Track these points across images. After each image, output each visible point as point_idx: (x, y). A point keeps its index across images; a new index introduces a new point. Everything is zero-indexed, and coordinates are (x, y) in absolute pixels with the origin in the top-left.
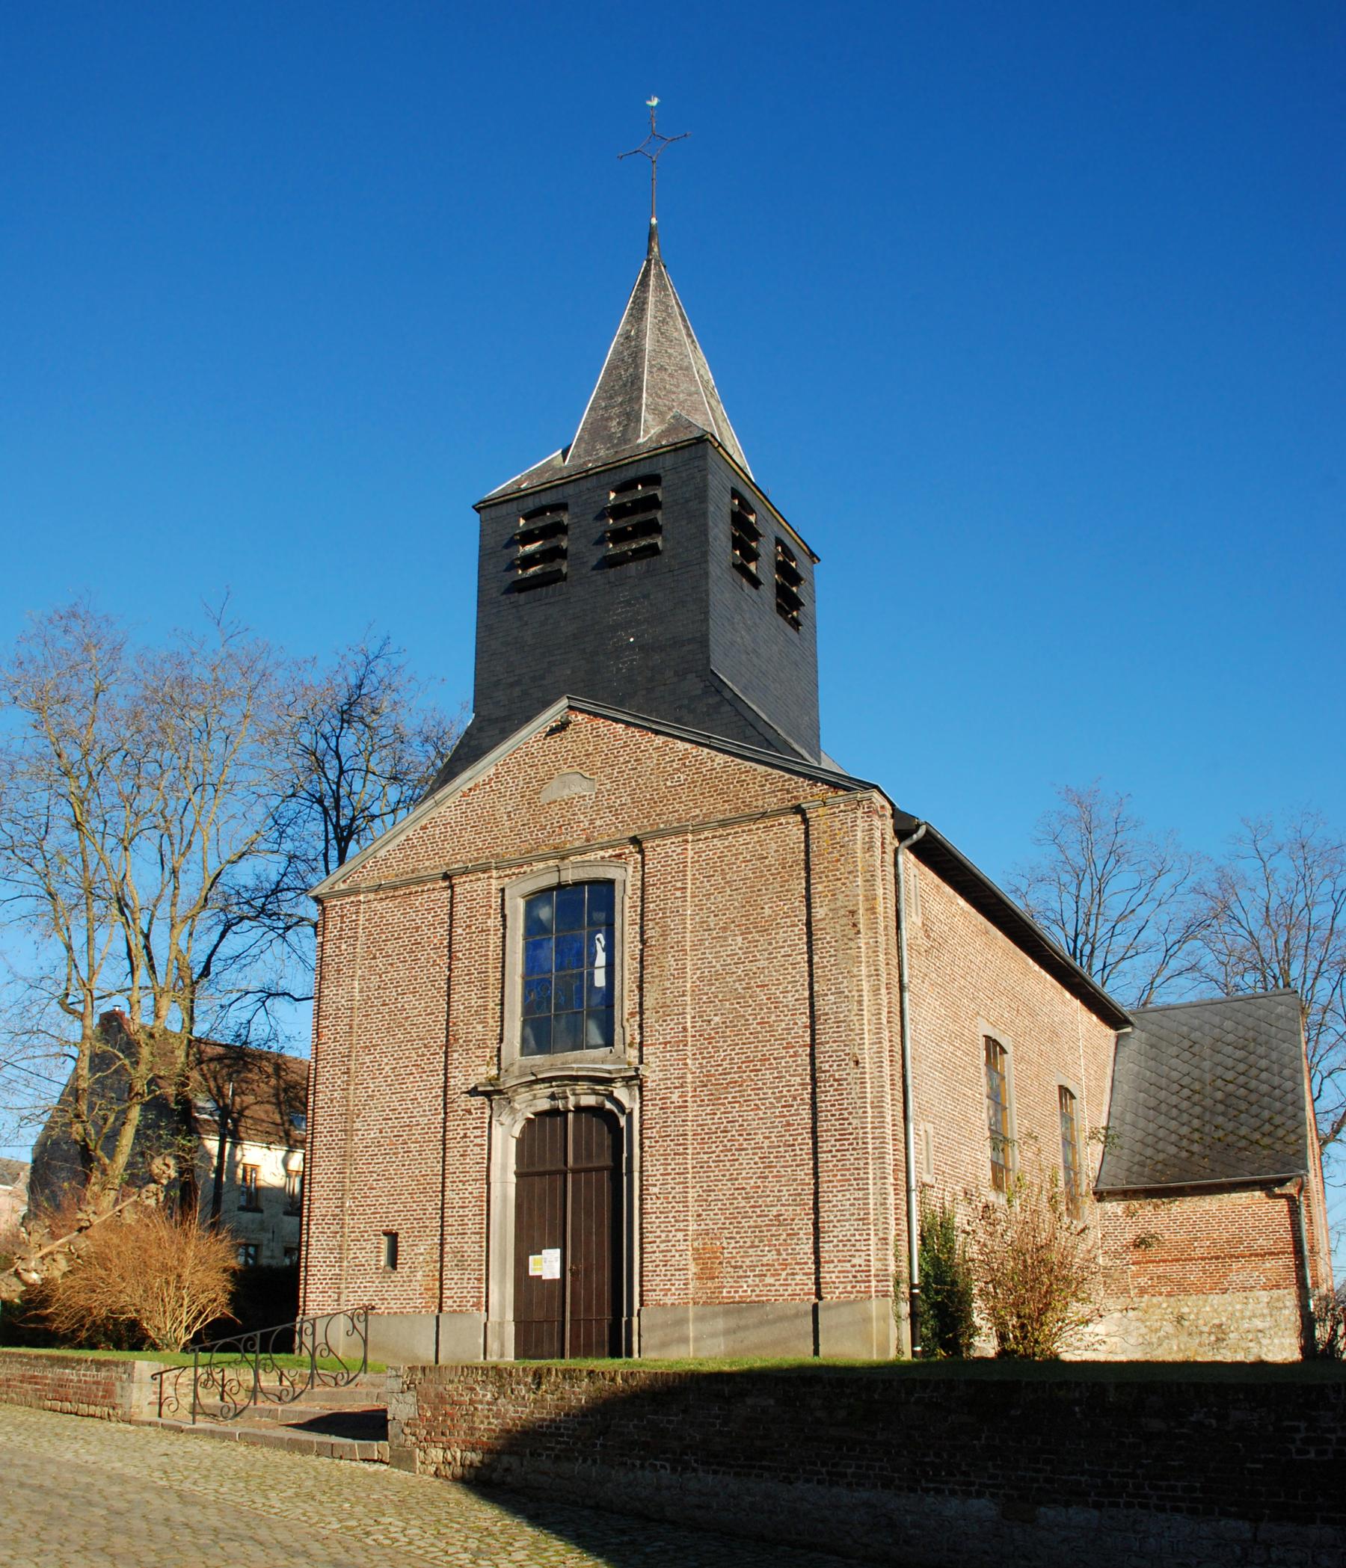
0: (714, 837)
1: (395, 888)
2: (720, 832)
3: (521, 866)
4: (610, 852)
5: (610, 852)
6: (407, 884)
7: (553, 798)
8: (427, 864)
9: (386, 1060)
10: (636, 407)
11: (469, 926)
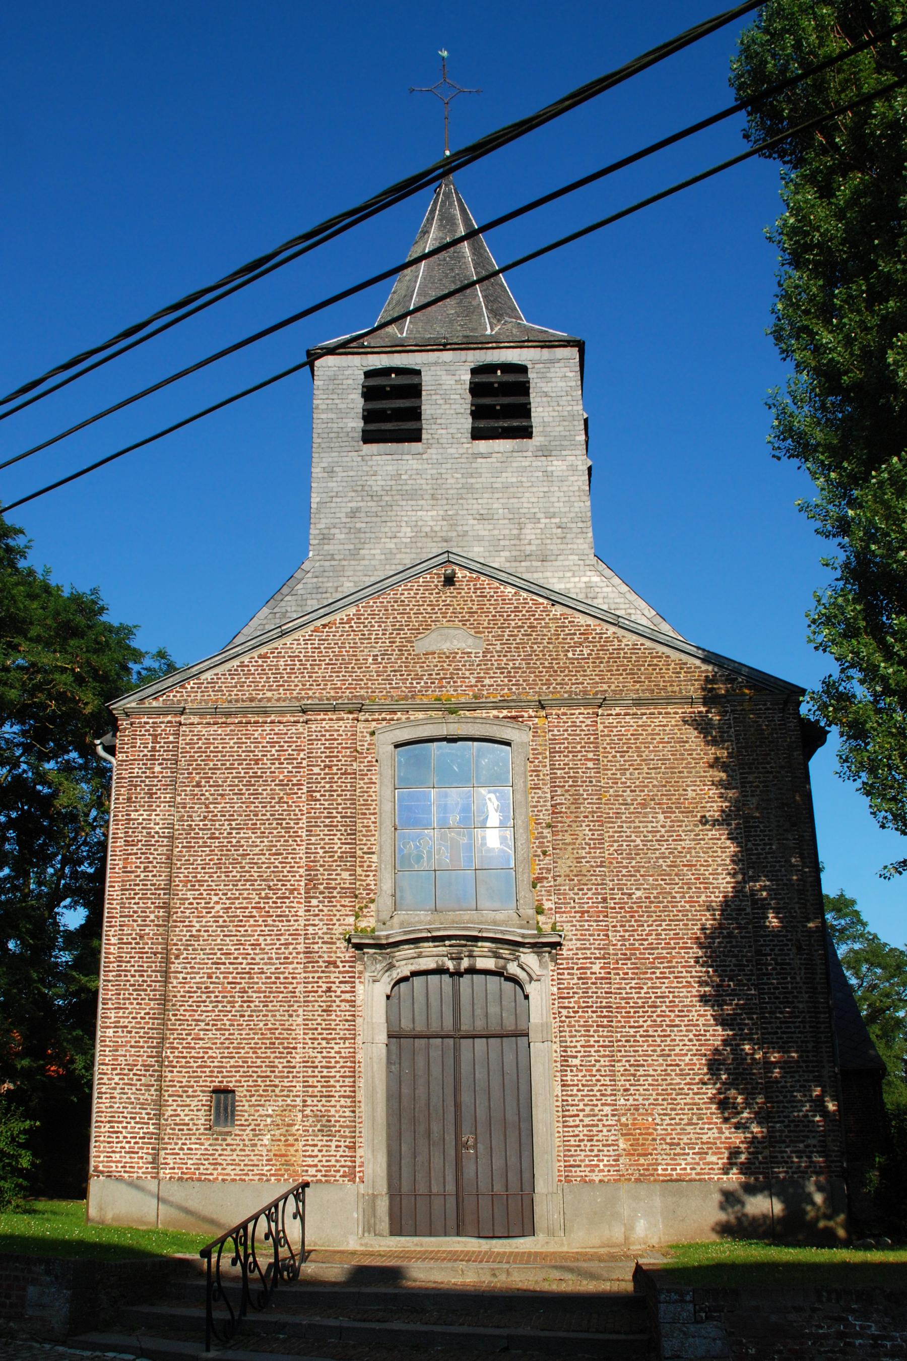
0: (626, 714)
1: (228, 714)
3: (395, 712)
4: (505, 713)
5: (505, 713)
6: (245, 712)
7: (430, 650)
8: (269, 694)
9: (215, 899)
10: (474, 303)
11: (330, 767)
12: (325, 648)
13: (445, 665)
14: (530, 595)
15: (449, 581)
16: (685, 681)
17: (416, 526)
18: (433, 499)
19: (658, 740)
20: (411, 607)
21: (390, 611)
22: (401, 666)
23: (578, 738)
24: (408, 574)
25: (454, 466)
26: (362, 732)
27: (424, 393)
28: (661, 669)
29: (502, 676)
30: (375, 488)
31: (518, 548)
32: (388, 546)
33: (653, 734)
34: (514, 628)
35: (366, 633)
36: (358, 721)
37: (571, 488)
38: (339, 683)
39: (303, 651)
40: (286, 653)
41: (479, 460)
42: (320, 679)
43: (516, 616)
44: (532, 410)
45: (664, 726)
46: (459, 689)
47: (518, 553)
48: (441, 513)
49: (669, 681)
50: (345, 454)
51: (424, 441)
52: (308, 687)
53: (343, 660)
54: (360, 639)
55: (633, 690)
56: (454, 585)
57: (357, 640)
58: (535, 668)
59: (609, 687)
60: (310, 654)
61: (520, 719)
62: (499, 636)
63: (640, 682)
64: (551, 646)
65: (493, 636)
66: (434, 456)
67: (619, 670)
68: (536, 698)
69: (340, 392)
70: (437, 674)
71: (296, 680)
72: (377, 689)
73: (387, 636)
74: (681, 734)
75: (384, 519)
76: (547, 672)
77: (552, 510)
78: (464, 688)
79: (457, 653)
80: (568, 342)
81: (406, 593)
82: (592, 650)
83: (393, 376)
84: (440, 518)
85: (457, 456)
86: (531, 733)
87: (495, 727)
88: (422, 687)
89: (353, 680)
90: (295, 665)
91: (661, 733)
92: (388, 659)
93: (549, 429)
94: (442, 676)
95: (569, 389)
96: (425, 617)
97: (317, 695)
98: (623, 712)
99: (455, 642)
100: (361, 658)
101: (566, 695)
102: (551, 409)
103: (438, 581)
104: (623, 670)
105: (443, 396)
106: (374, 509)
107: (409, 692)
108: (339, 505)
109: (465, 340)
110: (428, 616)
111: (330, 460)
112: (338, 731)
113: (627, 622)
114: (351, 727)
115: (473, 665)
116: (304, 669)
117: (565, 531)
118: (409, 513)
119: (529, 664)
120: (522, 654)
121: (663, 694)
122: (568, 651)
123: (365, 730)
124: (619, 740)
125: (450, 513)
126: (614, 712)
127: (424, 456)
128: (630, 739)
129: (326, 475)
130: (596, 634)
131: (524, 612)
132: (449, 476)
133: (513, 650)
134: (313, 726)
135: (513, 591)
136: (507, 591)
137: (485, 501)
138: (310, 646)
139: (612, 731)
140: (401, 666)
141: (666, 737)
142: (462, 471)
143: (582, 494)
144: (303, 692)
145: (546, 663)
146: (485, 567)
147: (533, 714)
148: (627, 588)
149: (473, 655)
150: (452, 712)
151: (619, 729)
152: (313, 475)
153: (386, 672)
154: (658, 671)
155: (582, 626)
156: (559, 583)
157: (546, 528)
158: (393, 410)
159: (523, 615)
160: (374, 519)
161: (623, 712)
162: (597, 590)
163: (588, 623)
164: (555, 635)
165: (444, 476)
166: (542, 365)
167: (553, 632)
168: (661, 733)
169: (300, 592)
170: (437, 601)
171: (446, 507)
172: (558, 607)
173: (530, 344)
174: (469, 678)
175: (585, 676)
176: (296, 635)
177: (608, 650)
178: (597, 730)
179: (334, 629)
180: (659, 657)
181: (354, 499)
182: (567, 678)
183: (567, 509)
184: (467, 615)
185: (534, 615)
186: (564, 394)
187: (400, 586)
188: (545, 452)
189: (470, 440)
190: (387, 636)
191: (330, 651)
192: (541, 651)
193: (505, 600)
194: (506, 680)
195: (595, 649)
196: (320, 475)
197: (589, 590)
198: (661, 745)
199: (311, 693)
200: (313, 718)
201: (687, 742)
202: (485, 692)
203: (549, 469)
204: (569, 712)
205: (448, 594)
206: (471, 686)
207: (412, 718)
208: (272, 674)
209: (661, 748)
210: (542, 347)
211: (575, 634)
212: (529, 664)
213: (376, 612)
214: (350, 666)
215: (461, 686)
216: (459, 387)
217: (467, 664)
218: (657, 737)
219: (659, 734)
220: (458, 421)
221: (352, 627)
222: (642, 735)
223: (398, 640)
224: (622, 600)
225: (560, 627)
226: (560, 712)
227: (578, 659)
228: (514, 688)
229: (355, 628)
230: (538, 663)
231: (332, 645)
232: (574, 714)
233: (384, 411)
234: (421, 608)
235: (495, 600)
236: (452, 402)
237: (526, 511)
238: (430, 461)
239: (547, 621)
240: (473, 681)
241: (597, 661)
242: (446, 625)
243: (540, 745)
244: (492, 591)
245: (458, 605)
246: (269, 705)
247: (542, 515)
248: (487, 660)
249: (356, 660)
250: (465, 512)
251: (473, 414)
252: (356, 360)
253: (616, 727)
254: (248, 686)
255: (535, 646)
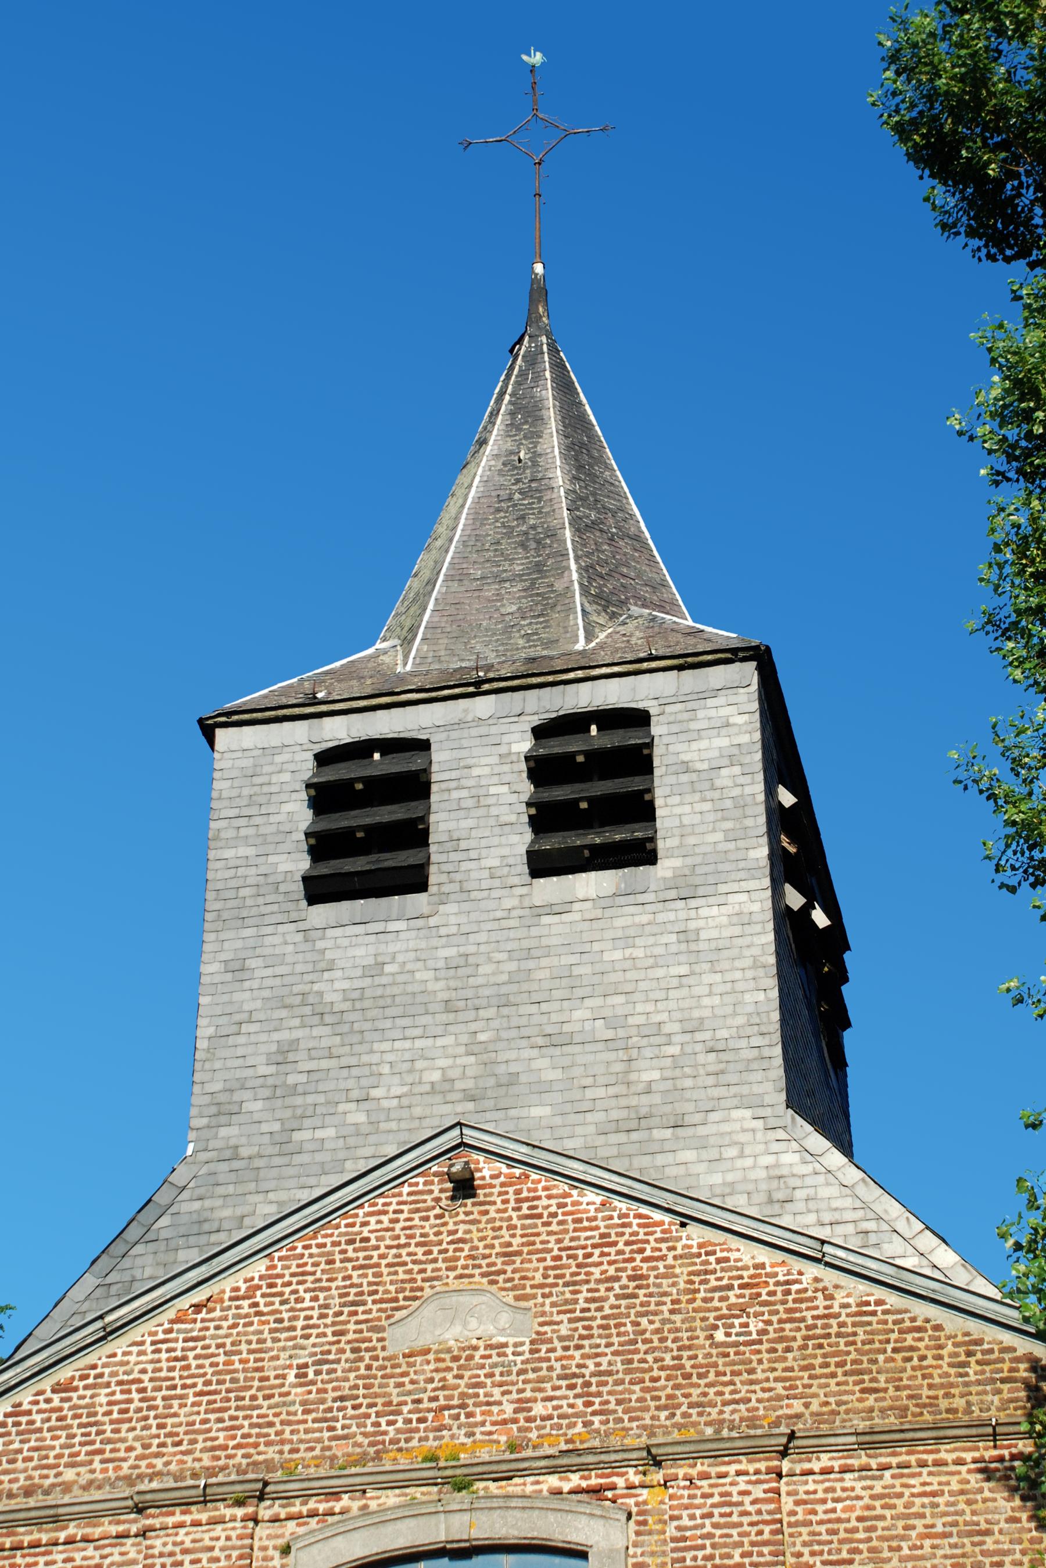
0: (845, 1470)
2: (862, 1459)
3: (336, 1495)
4: (575, 1480)
5: (575, 1480)
7: (420, 1344)
8: (69, 1475)
10: (559, 586)
12: (197, 1357)
13: (449, 1376)
14: (635, 1205)
15: (464, 1187)
16: (979, 1383)
17: (410, 1071)
18: (448, 1011)
19: (920, 1529)
20: (383, 1250)
21: (338, 1264)
22: (356, 1387)
23: (734, 1532)
24: (377, 1180)
25: (494, 936)
26: (264, 1549)
27: (434, 788)
28: (922, 1358)
29: (571, 1393)
30: (328, 998)
31: (623, 1102)
32: (351, 1118)
33: (908, 1517)
34: (599, 1281)
35: (285, 1315)
36: (256, 1521)
37: (738, 964)
38: (221, 1434)
39: (150, 1367)
40: (113, 1374)
41: (546, 920)
42: (181, 1430)
43: (602, 1254)
44: (658, 802)
45: (934, 1494)
46: (478, 1430)
47: (624, 1114)
48: (464, 1039)
49: (942, 1386)
50: (270, 930)
51: (432, 889)
52: (154, 1449)
53: (233, 1380)
54: (271, 1331)
55: (861, 1411)
56: (474, 1196)
57: (266, 1335)
58: (644, 1371)
59: (807, 1405)
60: (163, 1374)
61: (609, 1494)
62: (566, 1302)
63: (876, 1390)
64: (678, 1318)
65: (553, 1305)
66: (453, 920)
67: (827, 1365)
68: (644, 1440)
69: (262, 799)
70: (432, 1399)
71: (131, 1435)
72: (300, 1442)
73: (329, 1321)
74: (974, 1513)
75: (344, 1061)
76: (668, 1379)
77: (696, 1014)
78: (488, 1428)
79: (476, 1348)
80: (734, 651)
81: (373, 1220)
82: (768, 1323)
83: (377, 756)
84: (462, 1050)
85: (499, 914)
86: (632, 1526)
87: (551, 1517)
88: (398, 1431)
89: (251, 1426)
90: (130, 1401)
91: (928, 1511)
92: (329, 1372)
93: (692, 840)
94: (442, 1402)
95: (735, 751)
96: (410, 1272)
97: (173, 1467)
98: (836, 1465)
99: (473, 1323)
100: (272, 1374)
101: (709, 1431)
102: (697, 796)
103: (440, 1189)
104: (838, 1365)
105: (474, 792)
106: (325, 1043)
107: (372, 1444)
108: (253, 1038)
109: (522, 669)
110: (416, 1268)
111: (239, 944)
112: (212, 1549)
113: (841, 1253)
114: (240, 1537)
115: (509, 1373)
116: (149, 1408)
117: (723, 1056)
118: (398, 1045)
119: (630, 1361)
120: (615, 1340)
121: (927, 1417)
122: (715, 1327)
123: (270, 1543)
124: (830, 1532)
125: (482, 1037)
126: (816, 1466)
127: (433, 921)
128: (855, 1530)
129: (229, 976)
130: (778, 1284)
131: (621, 1246)
132: (481, 959)
133: (595, 1332)
134: (158, 1542)
135: (598, 1200)
136: (585, 1200)
137: (556, 1006)
138: (164, 1356)
139: (814, 1512)
140: (356, 1387)
141: (939, 1522)
142: (510, 946)
143: (761, 972)
144: (143, 1463)
145: (668, 1357)
146: (537, 1153)
147: (636, 1479)
148: (859, 1175)
149: (509, 1351)
150: (461, 1486)
151: (830, 1505)
152: (204, 980)
153: (323, 1401)
154: (915, 1362)
155: (746, 1268)
156: (710, 1172)
157: (683, 1053)
158: (367, 829)
159: (620, 1252)
160: (324, 1064)
161: (836, 1465)
162: (793, 1182)
163: (760, 1259)
164: (688, 1291)
165: (471, 960)
166: (679, 707)
167: (682, 1286)
168: (928, 1511)
169: (164, 1234)
170: (436, 1234)
171: (473, 1026)
172: (693, 1229)
173: (654, 665)
174: (500, 1403)
175: (752, 1382)
176: (136, 1333)
177: (803, 1320)
178: (779, 1510)
179: (217, 1314)
180: (919, 1329)
181: (285, 1023)
182: (712, 1391)
183: (729, 1010)
184: (499, 1261)
185: (642, 1251)
186: (725, 762)
187: (361, 1206)
188: (686, 892)
189: (527, 878)
190: (329, 1321)
191: (207, 1362)
192: (657, 1331)
193: (580, 1221)
194: (579, 1402)
195: (775, 1319)
196: (217, 979)
197: (775, 1184)
198: (927, 1543)
199: (159, 1463)
200: (156, 1522)
201: (988, 1533)
202: (533, 1435)
203: (692, 925)
204: (713, 1471)
205: (462, 1217)
206: (504, 1422)
207: (373, 1505)
208: (81, 1426)
209: (927, 1550)
210: (680, 668)
211: (730, 1287)
212: (630, 1361)
213: (309, 1268)
214: (248, 1394)
215: (483, 1424)
216: (506, 768)
217: (497, 1371)
218: (919, 1523)
219: (923, 1516)
220: (503, 840)
221: (256, 1305)
222: (882, 1518)
223: (352, 1327)
224: (848, 1202)
225: (697, 1273)
226: (694, 1472)
227: (736, 1344)
228: (596, 1419)
229: (262, 1308)
230: (650, 1358)
231: (213, 1350)
232: (724, 1475)
233: (350, 831)
234: (404, 1252)
235: (560, 1223)
236: (491, 801)
237: (641, 1020)
238: (443, 931)
239: (670, 1261)
240: (509, 1409)
241: (780, 1347)
242: (456, 1284)
243: (653, 1554)
244: (553, 1202)
245: (481, 1239)
246: (67, 1499)
247: (676, 1027)
248: (541, 1360)
249: (262, 1379)
250: (514, 1033)
251: (533, 821)
252: (299, 731)
253: (824, 1501)
254: (25, 1460)
255: (644, 1321)
